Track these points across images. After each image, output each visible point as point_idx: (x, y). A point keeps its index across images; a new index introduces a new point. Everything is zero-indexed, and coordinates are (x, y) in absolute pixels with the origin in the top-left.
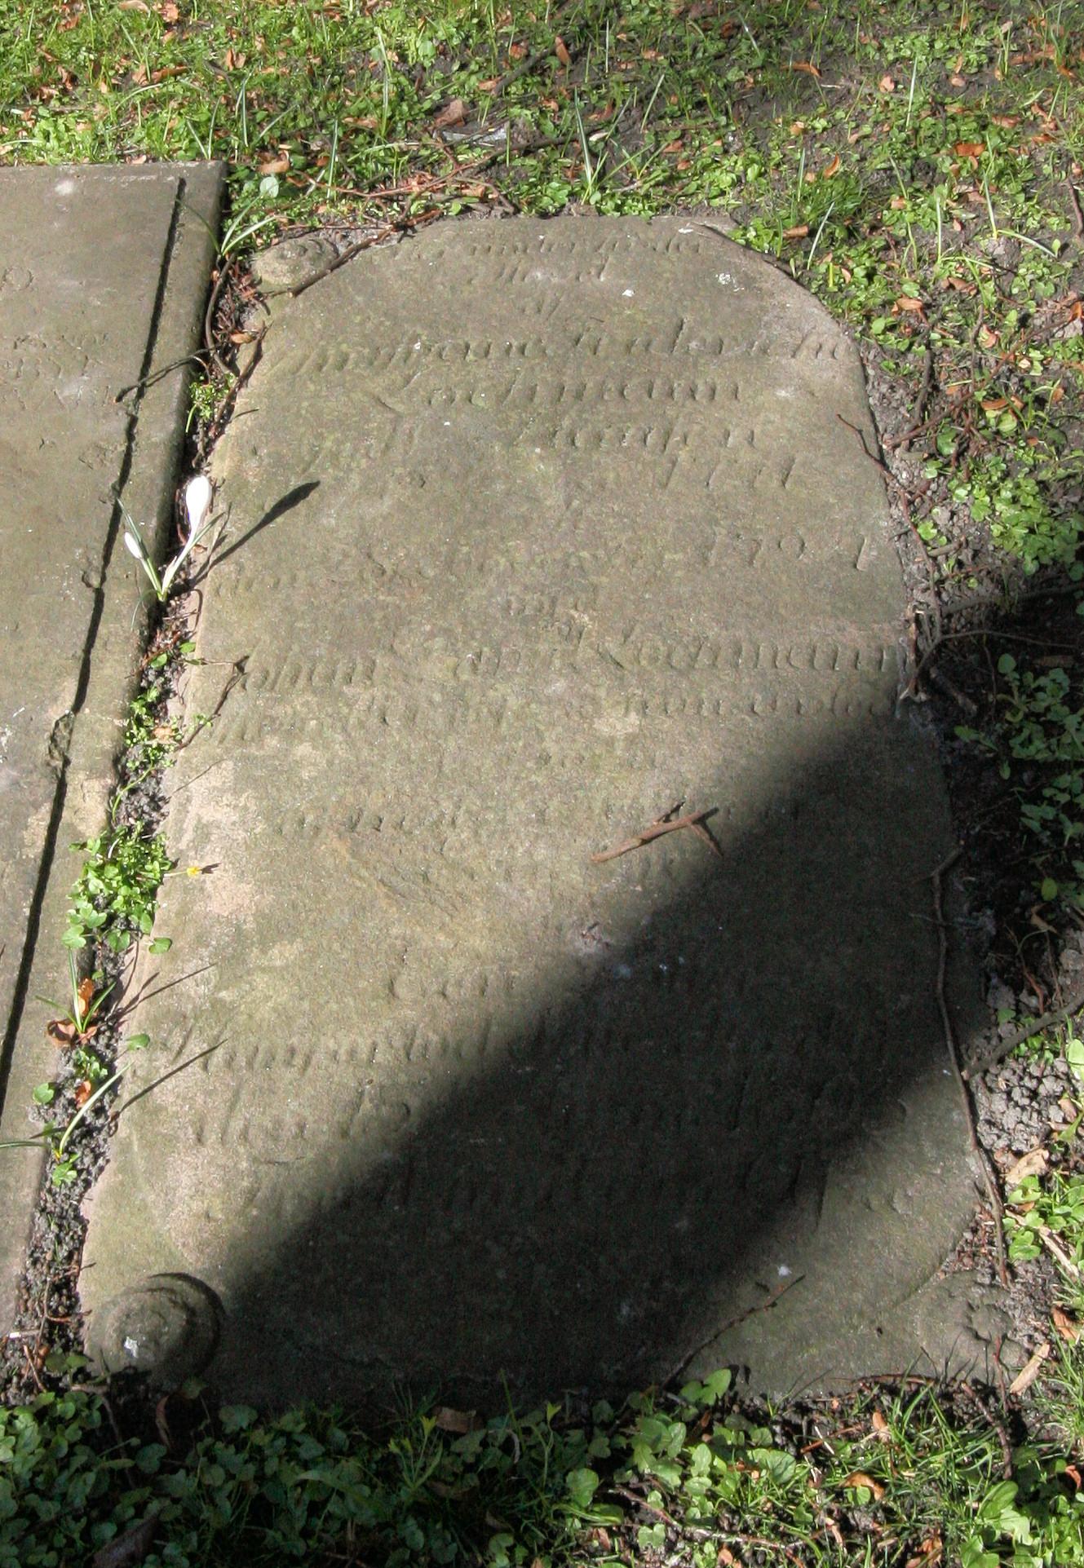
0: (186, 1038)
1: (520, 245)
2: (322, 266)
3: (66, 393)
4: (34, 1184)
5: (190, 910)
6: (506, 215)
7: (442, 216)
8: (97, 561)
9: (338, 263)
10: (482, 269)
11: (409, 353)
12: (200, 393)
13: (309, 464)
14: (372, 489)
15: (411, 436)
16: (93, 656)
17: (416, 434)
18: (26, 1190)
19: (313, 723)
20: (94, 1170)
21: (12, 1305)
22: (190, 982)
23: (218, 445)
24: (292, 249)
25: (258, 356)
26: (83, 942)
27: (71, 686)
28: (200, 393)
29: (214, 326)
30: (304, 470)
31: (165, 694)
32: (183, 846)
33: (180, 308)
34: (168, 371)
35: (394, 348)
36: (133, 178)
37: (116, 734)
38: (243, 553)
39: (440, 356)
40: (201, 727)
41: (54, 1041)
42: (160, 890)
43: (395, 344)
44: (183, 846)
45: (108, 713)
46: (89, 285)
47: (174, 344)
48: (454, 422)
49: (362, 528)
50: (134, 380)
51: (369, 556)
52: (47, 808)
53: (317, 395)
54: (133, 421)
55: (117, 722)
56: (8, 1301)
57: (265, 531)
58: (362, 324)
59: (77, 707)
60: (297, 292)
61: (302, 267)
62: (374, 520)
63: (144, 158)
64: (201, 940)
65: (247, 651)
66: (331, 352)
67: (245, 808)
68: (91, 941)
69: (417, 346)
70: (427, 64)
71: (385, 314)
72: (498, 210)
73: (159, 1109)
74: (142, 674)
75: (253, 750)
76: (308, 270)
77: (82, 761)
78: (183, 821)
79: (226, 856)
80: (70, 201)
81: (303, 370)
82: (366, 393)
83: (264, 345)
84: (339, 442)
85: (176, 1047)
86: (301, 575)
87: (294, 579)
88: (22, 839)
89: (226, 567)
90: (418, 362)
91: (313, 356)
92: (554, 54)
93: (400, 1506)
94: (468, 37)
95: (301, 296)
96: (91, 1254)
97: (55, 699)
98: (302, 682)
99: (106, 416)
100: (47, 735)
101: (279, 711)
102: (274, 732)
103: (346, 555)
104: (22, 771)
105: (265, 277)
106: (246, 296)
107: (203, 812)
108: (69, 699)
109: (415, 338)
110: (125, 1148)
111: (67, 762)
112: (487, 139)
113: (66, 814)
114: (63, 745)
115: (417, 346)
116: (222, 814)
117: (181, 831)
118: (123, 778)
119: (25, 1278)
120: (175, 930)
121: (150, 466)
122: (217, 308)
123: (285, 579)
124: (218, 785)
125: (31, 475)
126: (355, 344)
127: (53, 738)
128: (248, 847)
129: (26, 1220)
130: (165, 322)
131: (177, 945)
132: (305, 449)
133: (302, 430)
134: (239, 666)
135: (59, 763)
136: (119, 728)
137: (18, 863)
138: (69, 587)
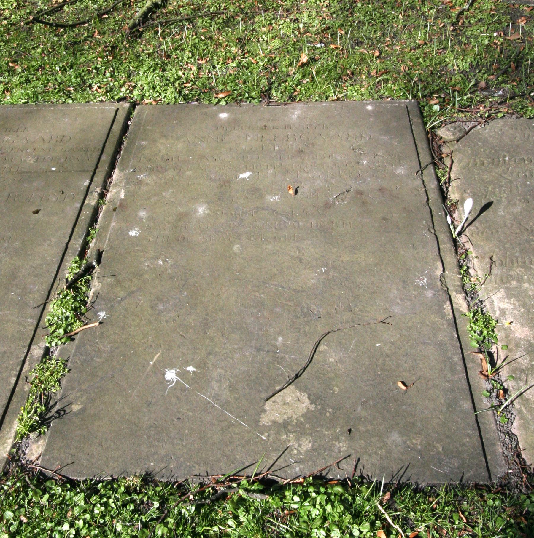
0: (527, 376)
1: (527, 127)
2: (463, 133)
3: (398, 172)
4: (494, 423)
5: (509, 336)
6: (517, 118)
7: (495, 118)
8: (431, 225)
9: (467, 133)
10: (518, 135)
11: (505, 161)
12: (440, 172)
13: (486, 195)
14: (511, 203)
15: (517, 187)
16: (441, 255)
17: (519, 186)
18: (493, 425)
19: (526, 277)
20: (512, 418)
21: (504, 462)
22: (520, 359)
23: (450, 189)
24: (451, 127)
25: (452, 162)
26: (478, 345)
27: (439, 264)
28: (440, 172)
29: (433, 150)
30: (485, 197)
31: (468, 268)
32: (497, 315)
33: (423, 146)
34: (427, 165)
35: (499, 159)
36: (390, 105)
37: (460, 280)
38: (476, 223)
39: (515, 161)
40: (487, 278)
41: (482, 377)
42: (495, 329)
43: (498, 158)
44: (497, 315)
45: (455, 273)
46: (391, 138)
47: (426, 158)
48: (530, 182)
49: (514, 215)
50: (418, 168)
51: (520, 224)
52: (448, 303)
53: (478, 174)
54: (423, 181)
55: (459, 276)
56: (502, 461)
57: (480, 217)
58: (484, 151)
59: (444, 271)
60: (458, 141)
61: (456, 134)
62: (517, 213)
63: (390, 99)
64: (517, 345)
65: (492, 254)
66: (478, 160)
67: (514, 304)
68: (480, 345)
69: (507, 159)
70: (468, 70)
71: (491, 148)
72: (514, 116)
73: (527, 400)
74: (459, 261)
75: (508, 285)
76: (458, 135)
77: (452, 288)
78: (494, 308)
79: (514, 319)
80: (373, 111)
81: (470, 165)
82: (496, 173)
83: (453, 158)
84: (494, 189)
85: (525, 379)
86: (500, 230)
87: (497, 232)
88: (444, 313)
89: (472, 227)
90: (509, 164)
91: (472, 161)
92: (510, 67)
93: (258, 479)
94: (478, 62)
95: (459, 143)
96: (523, 446)
97: (436, 269)
98: (515, 264)
99: (414, 179)
100: (438, 280)
101: (511, 273)
102: (513, 280)
103: (513, 224)
104: (435, 291)
105: (444, 136)
106: (439, 143)
107: (500, 305)
108: (441, 269)
109: (504, 156)
110: (520, 412)
111: (448, 289)
112: (496, 94)
113: (454, 305)
114: (444, 283)
115: (507, 159)
116: (506, 305)
117: (494, 312)
118: (466, 293)
119: (504, 453)
120: (507, 342)
121: (434, 195)
122: (433, 147)
123: (494, 231)
124: (501, 296)
125: (398, 198)
126: (485, 158)
127: (440, 280)
128: (521, 317)
129: (497, 434)
130: (420, 150)
131: (510, 347)
132: (483, 191)
133: (479, 185)
134: (491, 259)
135: (446, 289)
136: (460, 278)
137: (447, 320)
138: (426, 233)
